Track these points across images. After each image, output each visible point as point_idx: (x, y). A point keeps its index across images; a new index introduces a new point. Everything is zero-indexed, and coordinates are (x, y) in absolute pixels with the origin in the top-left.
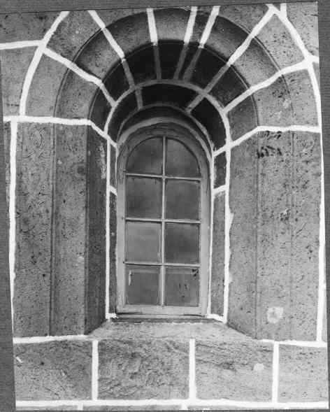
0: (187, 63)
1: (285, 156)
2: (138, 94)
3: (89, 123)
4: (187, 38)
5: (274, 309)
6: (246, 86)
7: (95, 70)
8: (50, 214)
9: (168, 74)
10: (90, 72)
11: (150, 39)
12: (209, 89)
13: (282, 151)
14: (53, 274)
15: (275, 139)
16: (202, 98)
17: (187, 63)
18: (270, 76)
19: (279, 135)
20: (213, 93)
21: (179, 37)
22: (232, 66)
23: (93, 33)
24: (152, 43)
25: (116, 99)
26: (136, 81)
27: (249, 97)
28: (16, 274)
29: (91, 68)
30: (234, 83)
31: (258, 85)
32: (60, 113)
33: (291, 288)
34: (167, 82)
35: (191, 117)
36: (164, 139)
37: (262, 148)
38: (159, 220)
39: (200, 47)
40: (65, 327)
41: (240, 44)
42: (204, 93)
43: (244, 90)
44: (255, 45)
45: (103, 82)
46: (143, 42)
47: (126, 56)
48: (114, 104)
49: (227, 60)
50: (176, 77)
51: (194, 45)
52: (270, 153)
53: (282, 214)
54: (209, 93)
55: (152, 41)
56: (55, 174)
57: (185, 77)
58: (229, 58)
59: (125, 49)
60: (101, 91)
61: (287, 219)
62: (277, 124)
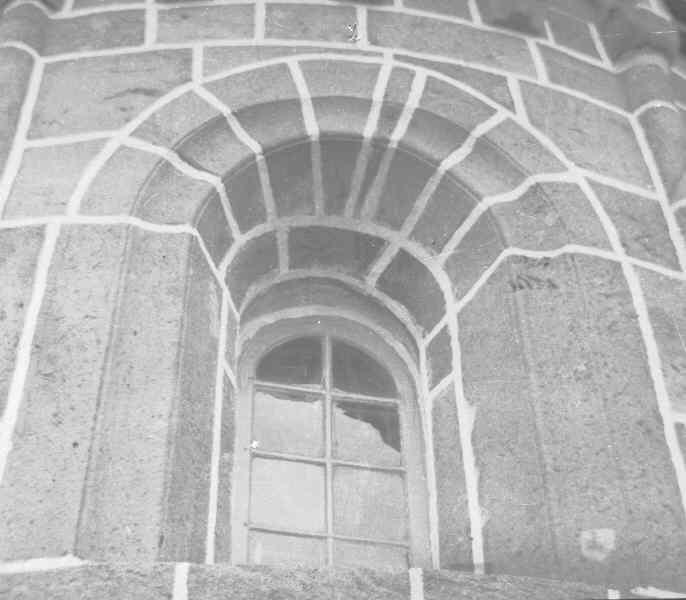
0: (371, 172)
1: (563, 289)
2: (282, 239)
3: (195, 233)
4: (370, 129)
5: (593, 533)
6: (475, 199)
7: (210, 165)
8: (103, 347)
9: (335, 205)
10: (199, 168)
11: (305, 131)
12: (409, 226)
13: (557, 282)
14: (96, 442)
15: (541, 267)
16: (395, 251)
17: (371, 172)
18: (515, 185)
19: (546, 262)
20: (415, 235)
21: (356, 129)
22: (448, 172)
23: (209, 118)
24: (308, 137)
25: (244, 229)
26: (281, 212)
27: (484, 214)
28: (15, 445)
29: (203, 164)
30: (455, 197)
31: (494, 197)
32: (144, 214)
33: (623, 490)
34: (333, 222)
35: (376, 294)
36: (329, 470)
37: (519, 277)
38: (321, 460)
39: (390, 145)
40: (113, 548)
41: (459, 146)
42: (398, 240)
43: (471, 207)
44: (484, 146)
45: (223, 181)
46: (295, 133)
47: (265, 152)
48: (240, 239)
49: (438, 163)
50: (349, 211)
51: (379, 143)
52: (535, 286)
53: (576, 371)
54: (410, 238)
55: (309, 133)
56: (122, 290)
57: (363, 213)
58: (441, 160)
59: (263, 142)
60: (218, 194)
61: (589, 376)
62: (541, 247)
